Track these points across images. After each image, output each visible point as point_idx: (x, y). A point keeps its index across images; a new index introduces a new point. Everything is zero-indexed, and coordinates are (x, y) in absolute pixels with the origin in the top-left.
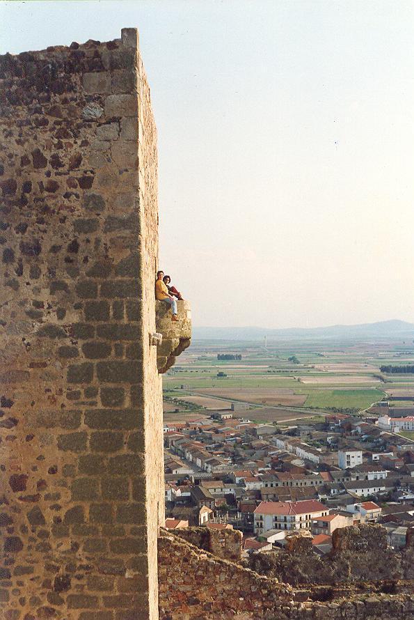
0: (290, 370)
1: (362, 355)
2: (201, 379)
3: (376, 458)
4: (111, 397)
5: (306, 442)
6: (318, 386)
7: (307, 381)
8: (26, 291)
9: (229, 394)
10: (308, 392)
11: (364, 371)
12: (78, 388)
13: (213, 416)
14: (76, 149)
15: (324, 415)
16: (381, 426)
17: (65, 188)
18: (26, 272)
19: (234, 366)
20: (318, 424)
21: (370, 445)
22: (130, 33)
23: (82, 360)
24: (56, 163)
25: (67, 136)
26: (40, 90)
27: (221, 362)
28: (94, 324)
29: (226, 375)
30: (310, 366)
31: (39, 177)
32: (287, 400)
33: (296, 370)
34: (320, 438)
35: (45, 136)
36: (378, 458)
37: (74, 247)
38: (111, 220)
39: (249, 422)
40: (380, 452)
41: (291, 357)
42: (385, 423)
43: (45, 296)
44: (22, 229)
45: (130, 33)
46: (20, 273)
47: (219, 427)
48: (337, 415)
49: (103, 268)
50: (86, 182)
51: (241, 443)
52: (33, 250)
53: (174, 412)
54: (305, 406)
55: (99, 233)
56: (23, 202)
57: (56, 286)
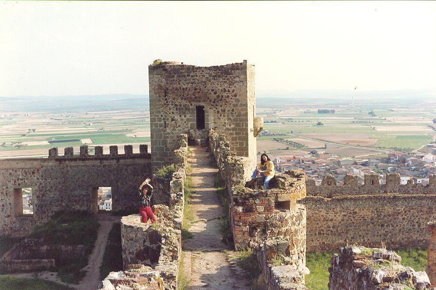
0: (368, 121)
1: (422, 111)
2: (306, 127)
3: (419, 181)
4: (241, 144)
5: (374, 170)
6: (386, 132)
7: (379, 129)
8: (222, 120)
9: (322, 137)
10: (379, 137)
11: (422, 122)
12: (234, 142)
13: (312, 152)
14: (233, 88)
15: (388, 152)
16: (426, 160)
17: (231, 97)
18: (222, 116)
19: (332, 118)
20: (383, 159)
21: (416, 173)
22: (245, 61)
23: (235, 136)
24: (229, 91)
25: (231, 85)
26: (225, 74)
27: (320, 115)
28: (237, 128)
29: (322, 124)
30: (383, 118)
31: (225, 94)
32: (363, 142)
33: (372, 121)
34: (383, 168)
35: (226, 85)
36: (421, 182)
37: (233, 110)
38: (241, 104)
39: (336, 156)
40: (422, 178)
41: (370, 111)
42: (429, 158)
43: (226, 121)
44: (221, 106)
45: (245, 61)
46: (221, 116)
47: (315, 160)
48: (396, 153)
49: (239, 115)
50: (235, 96)
51: (329, 170)
52: (224, 111)
53: (285, 149)
54: (376, 146)
55: (238, 107)
56: (221, 100)
57: (229, 119)
